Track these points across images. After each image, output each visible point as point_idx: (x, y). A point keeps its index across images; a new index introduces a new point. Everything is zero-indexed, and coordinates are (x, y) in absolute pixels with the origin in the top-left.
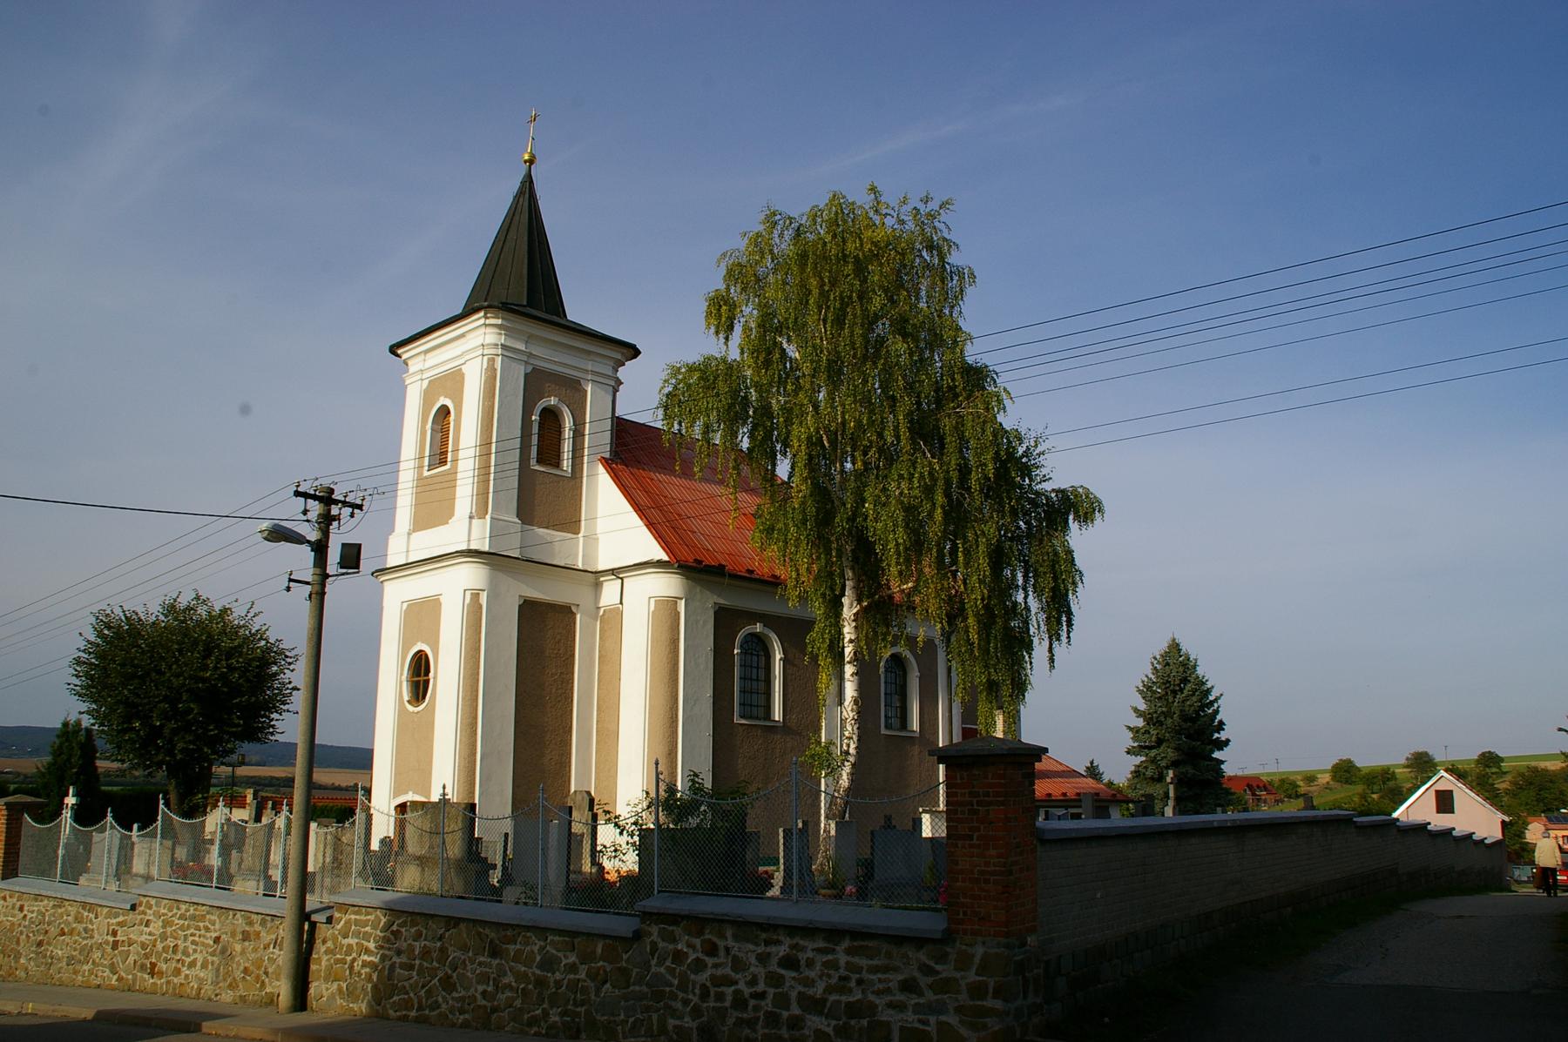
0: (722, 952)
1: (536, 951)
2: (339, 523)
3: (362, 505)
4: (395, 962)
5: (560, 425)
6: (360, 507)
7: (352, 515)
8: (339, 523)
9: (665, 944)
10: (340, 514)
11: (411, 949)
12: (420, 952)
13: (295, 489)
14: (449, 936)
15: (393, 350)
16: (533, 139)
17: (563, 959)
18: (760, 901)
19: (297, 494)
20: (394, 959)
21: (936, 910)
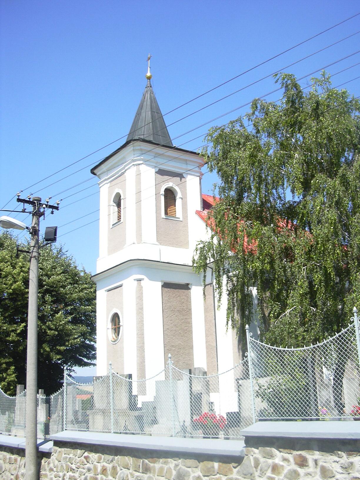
0: (311, 463)
1: (172, 468)
2: (44, 216)
3: (58, 207)
4: (87, 476)
5: (175, 196)
6: (57, 208)
7: (52, 213)
8: (44, 216)
9: (264, 459)
10: (44, 211)
11: (96, 468)
12: (101, 470)
13: (18, 197)
14: (117, 459)
15: (93, 171)
16: (150, 68)
17: (191, 473)
18: (216, 440)
19: (19, 200)
20: (86, 474)
21: (237, 439)
